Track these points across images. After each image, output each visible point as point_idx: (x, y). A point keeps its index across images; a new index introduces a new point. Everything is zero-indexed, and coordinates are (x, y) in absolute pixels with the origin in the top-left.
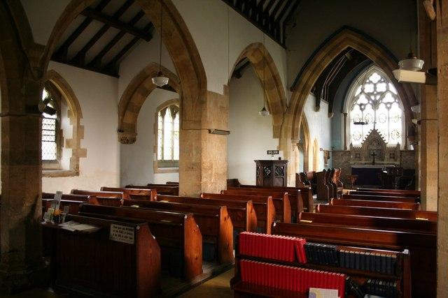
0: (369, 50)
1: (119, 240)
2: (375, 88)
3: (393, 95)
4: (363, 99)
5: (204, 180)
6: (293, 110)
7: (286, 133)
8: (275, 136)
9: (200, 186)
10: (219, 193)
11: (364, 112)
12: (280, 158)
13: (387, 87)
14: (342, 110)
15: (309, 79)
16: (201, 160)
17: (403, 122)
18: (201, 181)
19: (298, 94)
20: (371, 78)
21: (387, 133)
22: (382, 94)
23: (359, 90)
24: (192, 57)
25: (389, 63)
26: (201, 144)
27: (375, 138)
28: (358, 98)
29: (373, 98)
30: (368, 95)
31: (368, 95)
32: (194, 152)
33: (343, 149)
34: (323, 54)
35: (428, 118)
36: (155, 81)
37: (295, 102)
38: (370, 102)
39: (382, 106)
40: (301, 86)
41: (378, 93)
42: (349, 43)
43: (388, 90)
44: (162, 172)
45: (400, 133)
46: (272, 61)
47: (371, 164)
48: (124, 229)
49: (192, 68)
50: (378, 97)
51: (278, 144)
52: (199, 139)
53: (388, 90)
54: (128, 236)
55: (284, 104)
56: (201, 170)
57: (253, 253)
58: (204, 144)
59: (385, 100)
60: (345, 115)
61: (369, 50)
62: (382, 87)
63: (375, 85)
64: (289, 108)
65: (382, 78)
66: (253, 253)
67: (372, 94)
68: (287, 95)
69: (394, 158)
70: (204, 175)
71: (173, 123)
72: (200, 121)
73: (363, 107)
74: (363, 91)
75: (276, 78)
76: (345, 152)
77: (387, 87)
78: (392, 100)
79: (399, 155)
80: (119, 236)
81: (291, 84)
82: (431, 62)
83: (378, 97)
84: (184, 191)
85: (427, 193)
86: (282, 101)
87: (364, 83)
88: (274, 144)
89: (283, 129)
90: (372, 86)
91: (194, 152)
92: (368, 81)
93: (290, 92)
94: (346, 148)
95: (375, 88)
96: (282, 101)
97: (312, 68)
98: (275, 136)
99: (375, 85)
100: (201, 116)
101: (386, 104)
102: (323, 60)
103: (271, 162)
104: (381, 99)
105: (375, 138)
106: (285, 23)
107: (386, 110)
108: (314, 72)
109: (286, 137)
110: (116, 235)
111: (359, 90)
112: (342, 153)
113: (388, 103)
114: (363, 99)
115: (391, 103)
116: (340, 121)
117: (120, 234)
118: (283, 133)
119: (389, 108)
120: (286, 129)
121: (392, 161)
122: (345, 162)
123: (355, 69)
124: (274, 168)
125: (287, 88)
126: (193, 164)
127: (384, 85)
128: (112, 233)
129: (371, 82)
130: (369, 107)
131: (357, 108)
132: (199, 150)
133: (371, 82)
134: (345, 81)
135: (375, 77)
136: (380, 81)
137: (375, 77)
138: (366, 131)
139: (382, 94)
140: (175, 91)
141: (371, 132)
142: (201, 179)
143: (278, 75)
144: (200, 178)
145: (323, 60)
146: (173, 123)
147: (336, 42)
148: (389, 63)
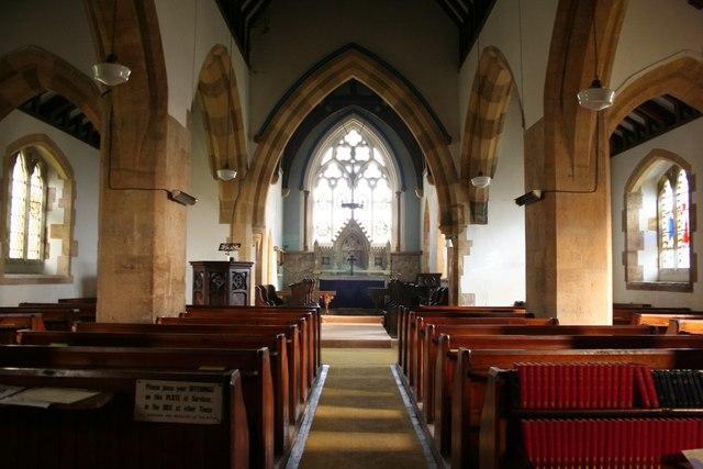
0: (387, 87)
1: (165, 419)
3: (380, 168)
4: (333, 170)
5: (158, 291)
6: (256, 176)
7: (243, 213)
10: (176, 316)
11: (336, 189)
12: (232, 259)
13: (371, 154)
14: (301, 186)
15: (286, 124)
16: (151, 249)
17: (393, 209)
18: (151, 292)
19: (267, 148)
20: (348, 138)
21: (370, 227)
22: (364, 165)
24: (146, 41)
25: (417, 112)
26: (153, 218)
27: (353, 235)
28: (324, 168)
29: (349, 169)
30: (342, 164)
31: (342, 164)
32: (137, 235)
33: (301, 249)
34: (313, 85)
35: (558, 188)
36: (104, 74)
37: (261, 162)
38: (345, 175)
39: (362, 183)
40: (272, 137)
41: (357, 162)
42: (355, 73)
43: (372, 159)
44: (14, 282)
45: (389, 224)
46: (235, 84)
48: (183, 389)
49: (144, 65)
50: (357, 169)
51: (228, 235)
52: (149, 208)
53: (372, 159)
54: (197, 405)
55: (244, 164)
57: (532, 403)
58: (159, 219)
60: (307, 193)
61: (387, 87)
62: (363, 154)
63: (353, 148)
64: (251, 170)
65: (363, 139)
66: (532, 403)
67: (349, 162)
69: (380, 264)
70: (158, 280)
71: (28, 184)
72: (153, 173)
73: (333, 182)
74: (334, 158)
75: (234, 116)
76: (307, 256)
77: (371, 154)
78: (377, 174)
79: (389, 259)
80: (166, 407)
81: (257, 129)
82: (562, 104)
83: (357, 169)
84: (112, 311)
85: (558, 303)
86: (239, 157)
87: (335, 144)
88: (223, 233)
89: (239, 207)
91: (137, 235)
92: (342, 142)
93: (253, 143)
94: (306, 247)
96: (239, 157)
97: (295, 104)
98: (223, 220)
99: (353, 148)
100: (154, 163)
101: (369, 180)
102: (311, 94)
104: (362, 171)
105: (353, 235)
106: (253, 21)
107: (369, 189)
108: (295, 112)
109: (244, 221)
110: (156, 407)
113: (332, 178)
114: (333, 170)
115: (376, 180)
116: (298, 203)
117: (156, 401)
118: (238, 216)
119: (373, 187)
120: (244, 207)
121: (377, 270)
123: (327, 120)
124: (231, 275)
125: (249, 136)
126: (133, 260)
127: (366, 150)
128: (140, 401)
129: (346, 144)
130: (343, 184)
131: (323, 183)
132: (149, 232)
133: (346, 144)
134: (307, 143)
135: (353, 137)
136: (360, 144)
137: (353, 137)
138: (341, 219)
139: (364, 165)
141: (347, 222)
142: (152, 287)
144: (150, 286)
145: (311, 94)
146: (28, 184)
147: (335, 68)
148: (417, 112)
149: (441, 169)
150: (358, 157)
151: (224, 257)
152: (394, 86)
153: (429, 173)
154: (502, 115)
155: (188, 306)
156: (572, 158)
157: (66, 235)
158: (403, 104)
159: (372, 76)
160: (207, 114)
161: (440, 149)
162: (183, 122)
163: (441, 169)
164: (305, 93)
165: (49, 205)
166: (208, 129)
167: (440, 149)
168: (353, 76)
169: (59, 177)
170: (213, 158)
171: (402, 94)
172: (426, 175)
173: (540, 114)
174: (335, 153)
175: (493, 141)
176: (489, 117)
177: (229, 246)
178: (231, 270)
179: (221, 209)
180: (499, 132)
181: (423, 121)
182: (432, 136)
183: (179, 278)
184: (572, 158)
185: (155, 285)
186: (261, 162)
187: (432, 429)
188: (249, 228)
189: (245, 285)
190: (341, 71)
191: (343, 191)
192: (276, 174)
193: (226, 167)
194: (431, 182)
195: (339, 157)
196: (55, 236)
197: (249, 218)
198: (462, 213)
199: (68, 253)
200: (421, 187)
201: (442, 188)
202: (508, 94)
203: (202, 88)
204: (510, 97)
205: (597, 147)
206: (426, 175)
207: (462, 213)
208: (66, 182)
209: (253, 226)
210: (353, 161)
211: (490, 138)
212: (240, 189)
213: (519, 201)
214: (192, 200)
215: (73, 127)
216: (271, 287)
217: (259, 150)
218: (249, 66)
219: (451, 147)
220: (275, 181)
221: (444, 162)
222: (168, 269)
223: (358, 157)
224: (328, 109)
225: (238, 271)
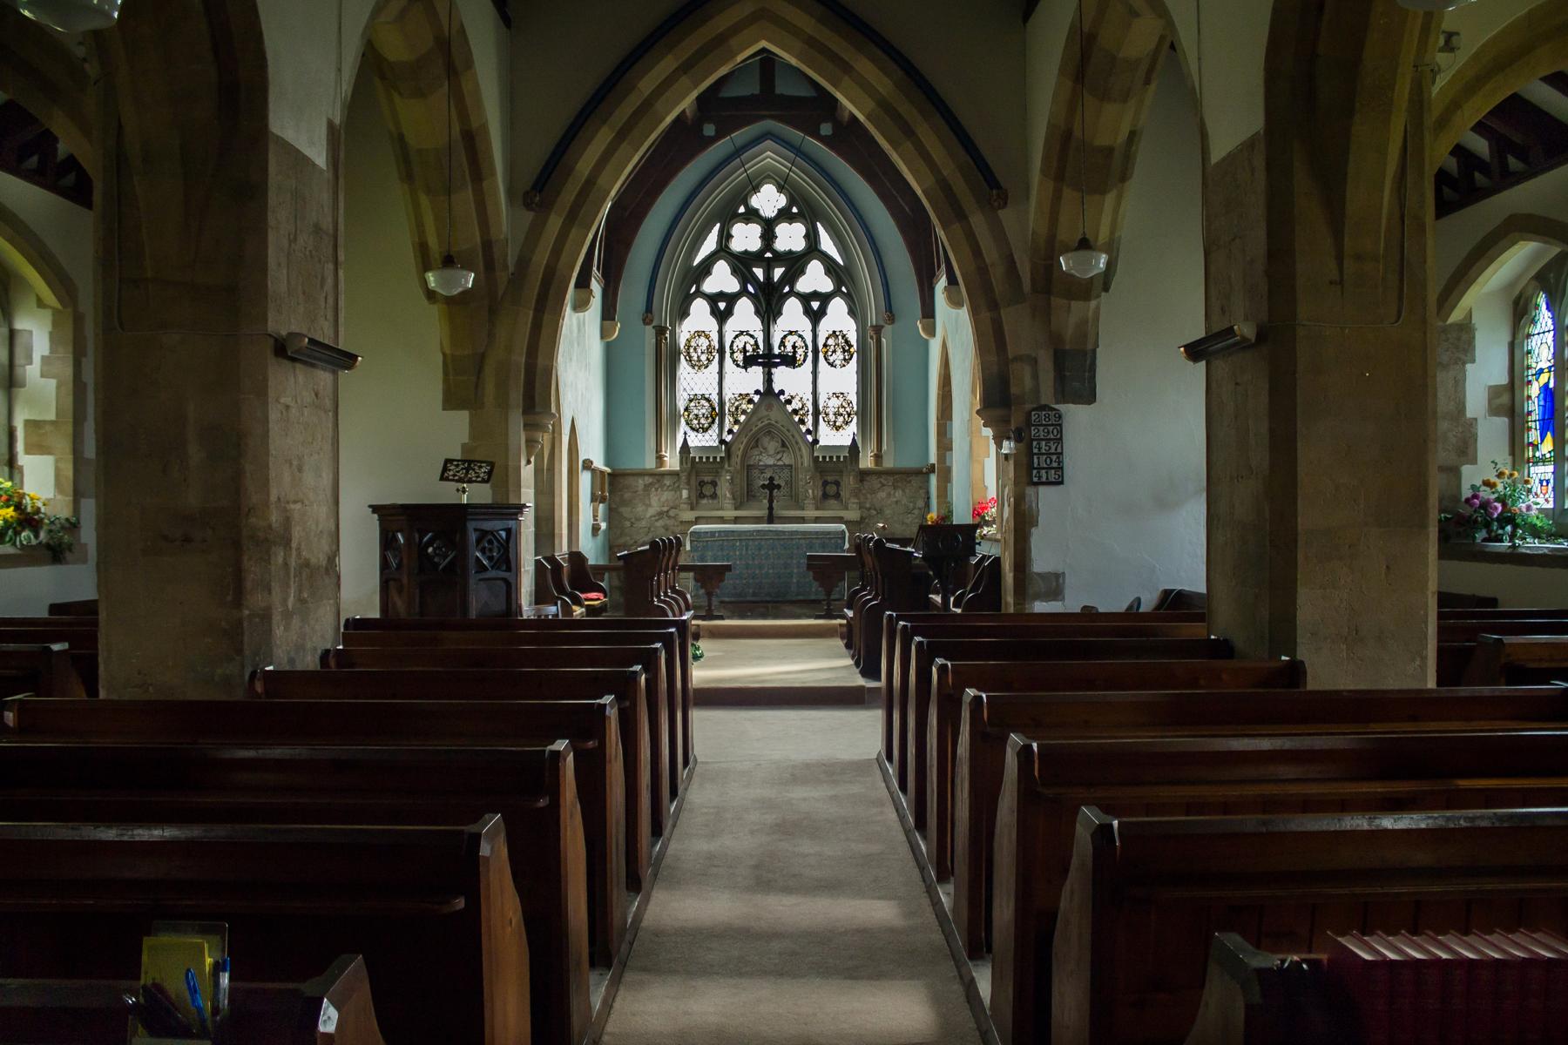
0: (847, 68)
2: (768, 236)
3: (831, 268)
4: (722, 279)
8: (451, 401)
9: (233, 636)
13: (812, 238)
18: (238, 602)
22: (795, 263)
23: (710, 244)
28: (706, 268)
30: (742, 264)
31: (742, 264)
32: (195, 453)
37: (541, 257)
39: (792, 315)
40: (569, 195)
43: (813, 249)
46: (469, 63)
47: (757, 520)
53: (813, 249)
56: (237, 545)
59: (804, 285)
61: (847, 68)
68: (506, 218)
74: (723, 251)
75: (472, 141)
83: (778, 273)
90: (755, 230)
91: (195, 453)
95: (768, 236)
96: (487, 245)
98: (451, 401)
103: (459, 513)
108: (622, 135)
109: (503, 404)
111: (710, 244)
112: (648, 480)
118: (490, 388)
122: (661, 514)
124: (473, 537)
125: (510, 192)
127: (799, 229)
136: (784, 215)
140: (462, 26)
143: (484, 128)
144: (234, 587)
149: (983, 270)
150: (781, 245)
151: (448, 494)
152: (865, 66)
153: (952, 280)
154: (1133, 135)
155: (353, 624)
156: (1338, 235)
157: (64, 444)
158: (886, 110)
159: (811, 42)
160: (401, 137)
161: (978, 221)
162: (319, 156)
163: (983, 270)
164: (647, 85)
165: (18, 371)
166: (408, 177)
167: (978, 221)
168: (764, 44)
169: (41, 304)
170: (423, 249)
171: (884, 84)
172: (941, 284)
173: (1254, 122)
174: (725, 237)
175: (1110, 199)
176: (1102, 140)
177: (456, 469)
178: (471, 526)
179: (446, 373)
180: (1124, 177)
181: (937, 152)
182: (960, 186)
183: (318, 557)
184: (1338, 235)
185: (248, 585)
186: (541, 257)
187: (945, 895)
188: (516, 420)
189: (506, 559)
190: (736, 29)
191: (656, 498)
192: (584, 283)
193: (449, 261)
194: (955, 302)
195: (737, 245)
196: (34, 448)
197: (516, 396)
198: (1035, 376)
199: (69, 488)
200: (928, 312)
201: (986, 315)
202: (1147, 81)
203: (373, 66)
204: (1153, 87)
205: (1402, 206)
206: (941, 284)
207: (1035, 376)
208: (56, 314)
209: (525, 412)
210: (767, 255)
211: (1103, 192)
212: (295, 377)
213: (1195, 351)
214: (347, 360)
215: (33, 161)
216: (577, 558)
217: (535, 231)
218: (506, 19)
219: (1007, 215)
220: (581, 305)
221: (991, 253)
222: (286, 542)
223: (781, 245)
224: (709, 130)
225: (487, 525)
